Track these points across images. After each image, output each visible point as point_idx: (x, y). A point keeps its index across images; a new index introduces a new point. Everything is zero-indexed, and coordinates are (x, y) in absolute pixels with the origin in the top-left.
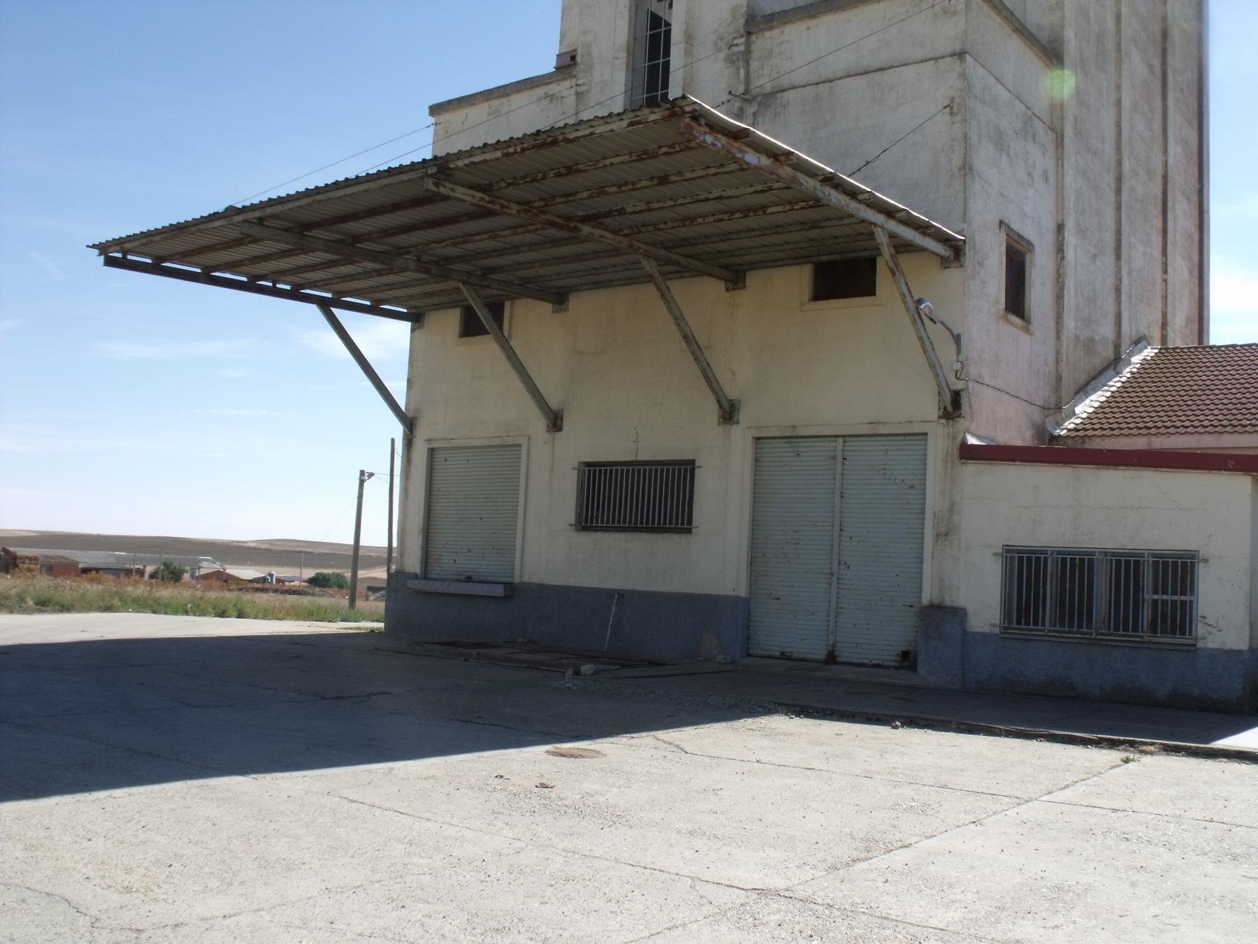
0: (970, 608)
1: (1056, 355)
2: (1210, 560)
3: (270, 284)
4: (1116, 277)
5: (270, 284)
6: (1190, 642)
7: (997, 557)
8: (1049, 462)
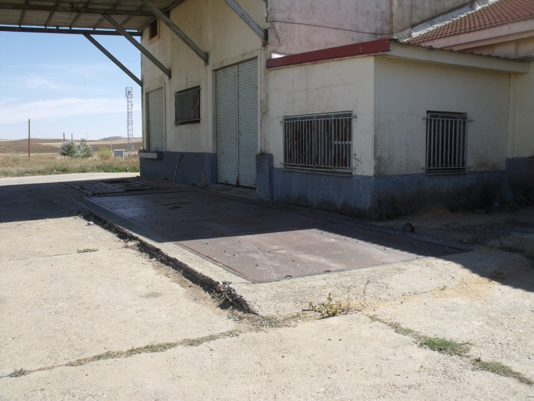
0: (274, 154)
2: (357, 116)
3: (56, 28)
5: (56, 28)
6: (349, 171)
7: (281, 123)
8: (295, 64)
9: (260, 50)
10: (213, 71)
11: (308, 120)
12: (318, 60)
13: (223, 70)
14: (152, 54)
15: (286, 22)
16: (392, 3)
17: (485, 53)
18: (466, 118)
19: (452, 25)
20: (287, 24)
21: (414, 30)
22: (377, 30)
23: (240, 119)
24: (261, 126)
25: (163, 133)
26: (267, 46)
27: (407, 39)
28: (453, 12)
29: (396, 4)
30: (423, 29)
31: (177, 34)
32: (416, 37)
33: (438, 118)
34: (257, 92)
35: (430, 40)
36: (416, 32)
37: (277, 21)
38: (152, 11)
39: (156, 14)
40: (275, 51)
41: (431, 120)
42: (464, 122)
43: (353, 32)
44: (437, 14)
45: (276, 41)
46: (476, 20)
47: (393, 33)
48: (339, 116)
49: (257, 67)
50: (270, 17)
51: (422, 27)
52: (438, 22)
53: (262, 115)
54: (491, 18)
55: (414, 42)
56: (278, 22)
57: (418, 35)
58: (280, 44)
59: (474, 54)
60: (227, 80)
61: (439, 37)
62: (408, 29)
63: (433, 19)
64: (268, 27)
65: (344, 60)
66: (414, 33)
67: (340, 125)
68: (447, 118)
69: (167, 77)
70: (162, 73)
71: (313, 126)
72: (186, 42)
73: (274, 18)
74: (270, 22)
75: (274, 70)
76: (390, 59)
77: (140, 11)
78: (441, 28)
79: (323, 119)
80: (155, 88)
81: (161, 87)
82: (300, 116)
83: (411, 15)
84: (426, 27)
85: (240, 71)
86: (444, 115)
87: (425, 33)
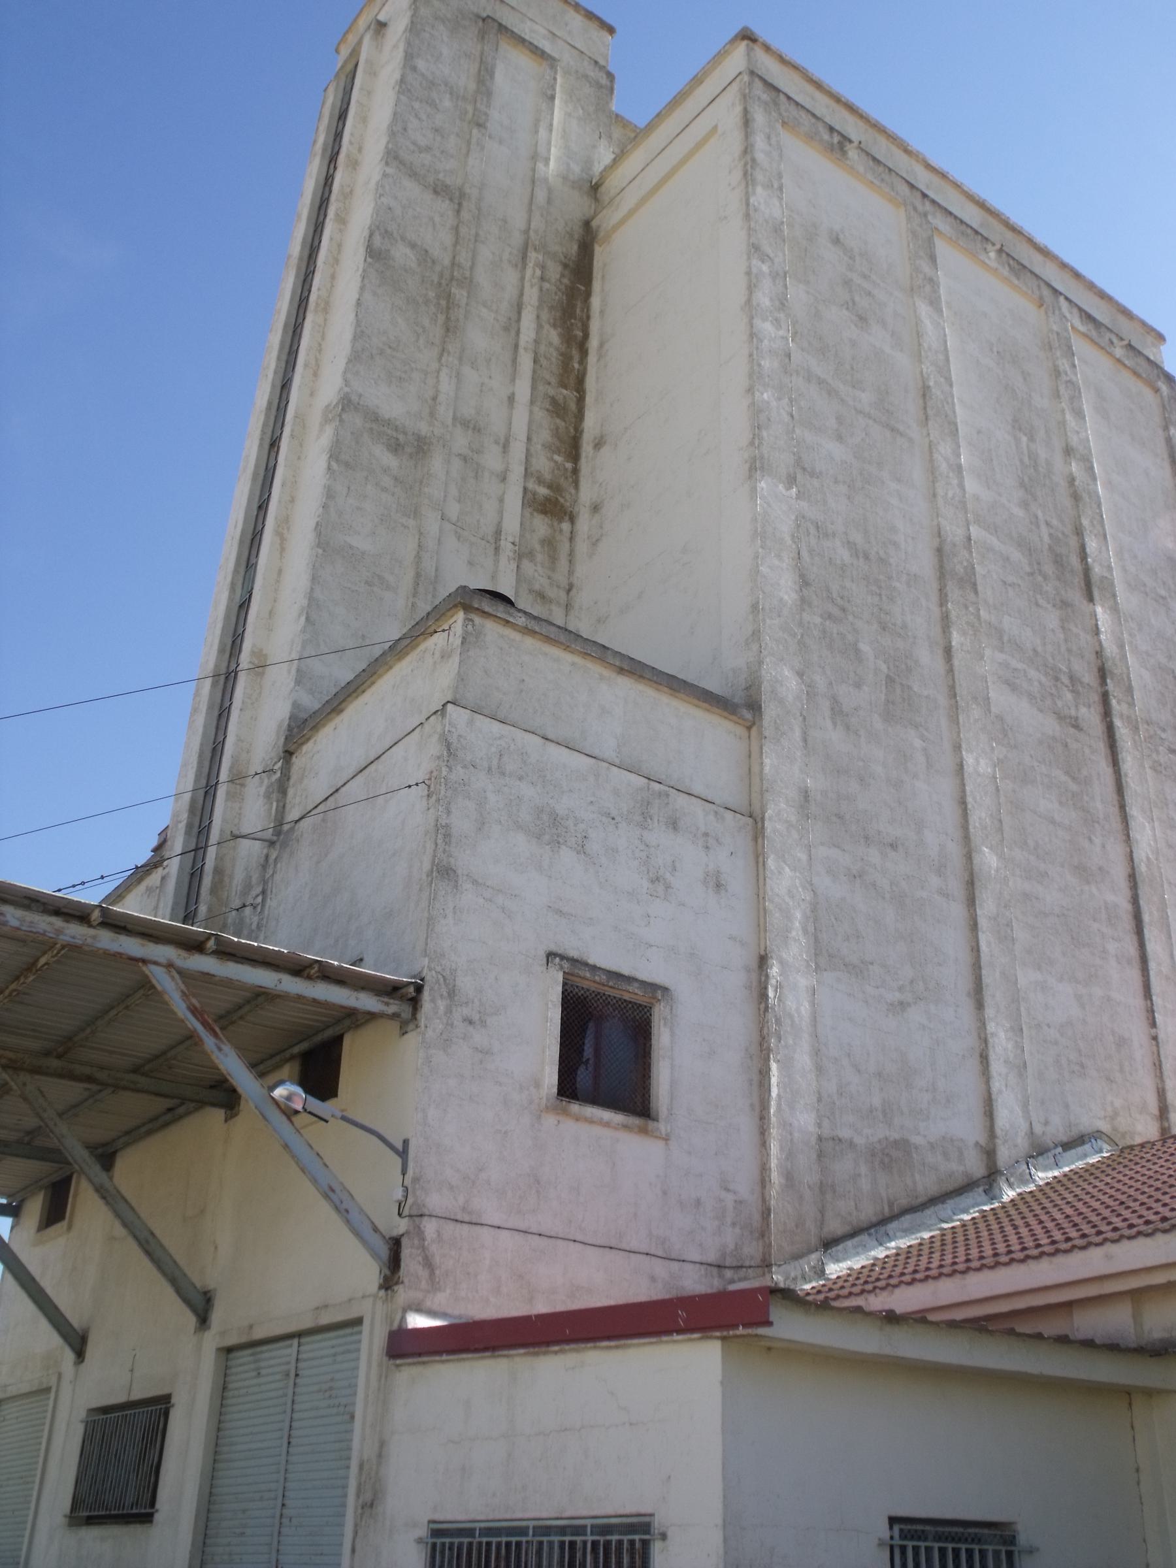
1: (762, 1173)
2: (669, 1534)
4: (980, 1038)
8: (476, 1350)
9: (371, 1300)
10: (219, 1350)
11: (509, 1539)
12: (548, 1343)
13: (249, 1351)
14: (38, 1278)
15: (456, 1221)
16: (767, 1179)
17: (1051, 1327)
18: (1011, 1540)
19: (943, 1245)
20: (459, 1225)
21: (832, 1257)
22: (724, 1255)
23: (285, 1521)
24: (353, 1551)
25: (21, 1549)
26: (396, 1288)
27: (810, 1281)
28: (940, 1206)
29: (777, 1182)
30: (858, 1254)
31: (125, 1225)
32: (838, 1277)
33: (926, 1540)
34: (352, 1431)
35: (883, 1289)
36: (838, 1261)
37: (430, 1216)
38: (61, 1148)
39: (70, 1159)
40: (419, 1304)
41: (903, 1549)
42: (1010, 1554)
43: (653, 1258)
44: (896, 1210)
45: (423, 1273)
46: (1009, 1229)
47: (769, 1266)
48: (606, 1529)
49: (358, 1350)
50: (410, 1201)
51: (855, 1247)
52: (898, 1234)
53: (360, 1511)
54: (1050, 1225)
55: (836, 1292)
56: (434, 1219)
57: (845, 1272)
58: (434, 1286)
59: (1019, 1335)
60: (260, 1385)
61: (907, 1278)
62: (813, 1252)
63: (886, 1224)
64: (401, 1230)
65: (629, 1346)
66: (832, 1265)
67: (613, 1560)
68: (953, 1540)
69: (70, 1356)
70: (56, 1340)
71: (523, 1560)
72: (148, 1253)
73: (424, 1205)
74: (410, 1216)
75: (409, 1364)
76: (769, 1349)
77: (28, 1143)
78: (909, 1252)
79: (556, 1539)
80: (25, 1388)
81: (44, 1386)
82: (483, 1525)
83: (822, 1212)
84: (866, 1248)
85: (305, 1360)
86: (943, 1533)
87: (863, 1267)
